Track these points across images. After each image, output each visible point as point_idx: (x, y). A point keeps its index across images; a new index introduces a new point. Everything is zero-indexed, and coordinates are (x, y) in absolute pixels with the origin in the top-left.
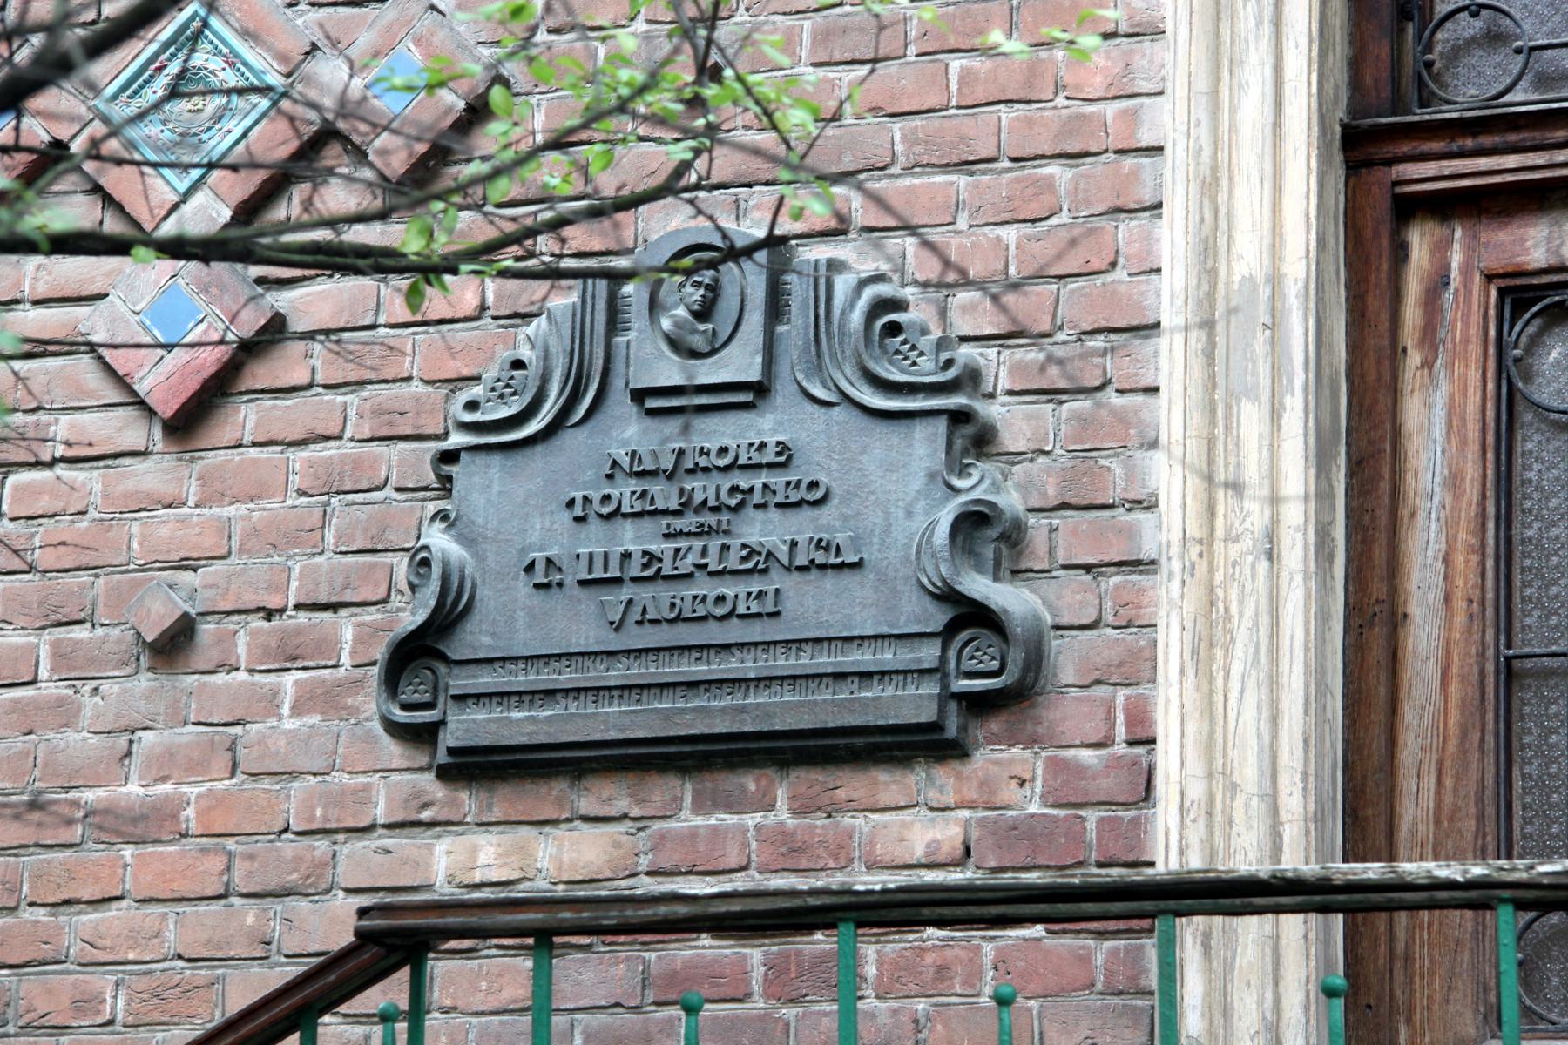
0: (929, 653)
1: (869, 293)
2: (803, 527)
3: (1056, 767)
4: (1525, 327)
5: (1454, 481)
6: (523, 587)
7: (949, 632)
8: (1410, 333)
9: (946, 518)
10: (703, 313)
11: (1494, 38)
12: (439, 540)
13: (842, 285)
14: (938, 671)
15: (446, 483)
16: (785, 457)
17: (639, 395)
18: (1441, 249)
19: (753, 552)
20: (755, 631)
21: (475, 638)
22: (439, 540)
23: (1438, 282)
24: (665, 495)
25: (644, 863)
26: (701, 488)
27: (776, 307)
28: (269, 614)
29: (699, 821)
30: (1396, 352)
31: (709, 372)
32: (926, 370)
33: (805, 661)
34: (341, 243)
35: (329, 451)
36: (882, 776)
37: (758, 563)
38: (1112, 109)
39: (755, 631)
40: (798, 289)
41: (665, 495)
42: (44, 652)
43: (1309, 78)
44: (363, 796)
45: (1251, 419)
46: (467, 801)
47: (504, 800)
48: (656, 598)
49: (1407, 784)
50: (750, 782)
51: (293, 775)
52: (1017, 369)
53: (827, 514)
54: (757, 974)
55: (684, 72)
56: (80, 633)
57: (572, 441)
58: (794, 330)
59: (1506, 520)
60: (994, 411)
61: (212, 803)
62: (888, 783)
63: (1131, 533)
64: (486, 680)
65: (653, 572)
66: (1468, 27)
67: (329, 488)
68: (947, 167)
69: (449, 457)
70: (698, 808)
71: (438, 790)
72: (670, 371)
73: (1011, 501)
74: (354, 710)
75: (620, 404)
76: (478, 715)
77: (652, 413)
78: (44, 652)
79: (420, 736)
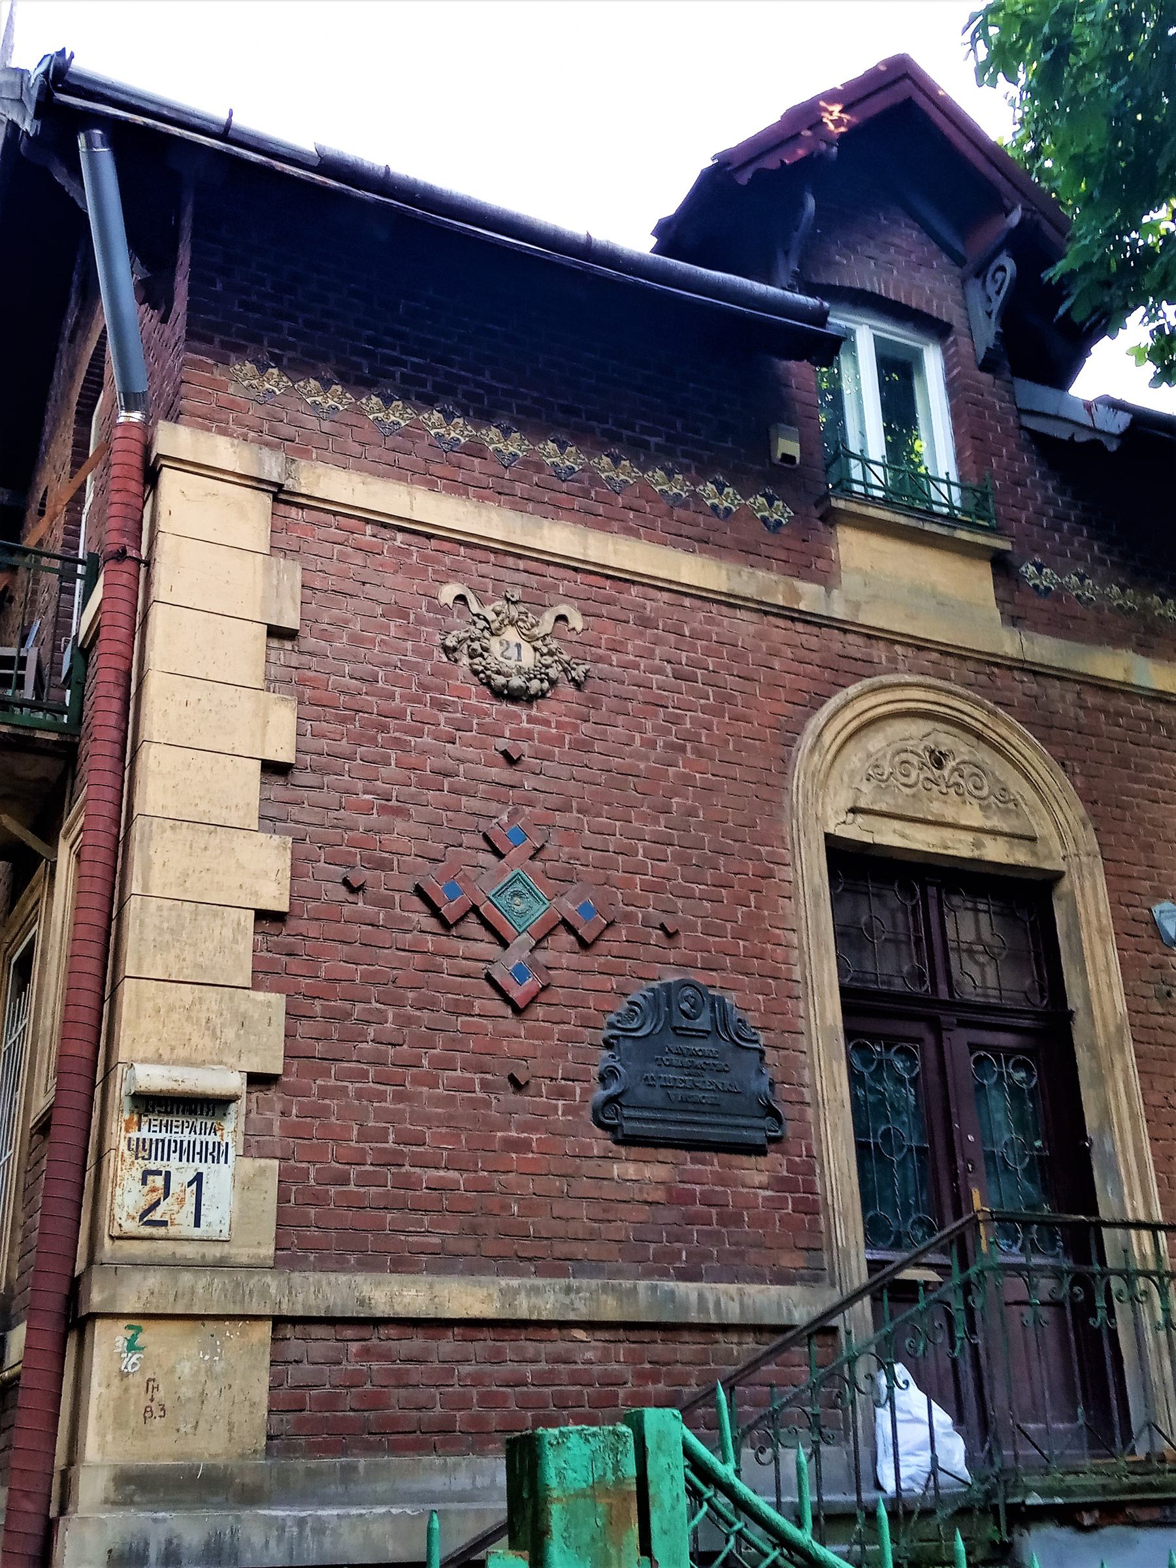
25: (678, 1179)
28: (552, 1079)
29: (692, 1167)
34: (1045, 1190)
35: (566, 1027)
36: (744, 1158)
38: (783, 966)
42: (477, 1081)
43: (850, 722)
46: (623, 1151)
47: (635, 1152)
50: (707, 1155)
51: (566, 1136)
54: (715, 1217)
56: (489, 1076)
62: (744, 1160)
67: (566, 1038)
68: (741, 974)
71: (614, 1147)
74: (581, 1116)
77: (678, 1035)
78: (477, 1081)
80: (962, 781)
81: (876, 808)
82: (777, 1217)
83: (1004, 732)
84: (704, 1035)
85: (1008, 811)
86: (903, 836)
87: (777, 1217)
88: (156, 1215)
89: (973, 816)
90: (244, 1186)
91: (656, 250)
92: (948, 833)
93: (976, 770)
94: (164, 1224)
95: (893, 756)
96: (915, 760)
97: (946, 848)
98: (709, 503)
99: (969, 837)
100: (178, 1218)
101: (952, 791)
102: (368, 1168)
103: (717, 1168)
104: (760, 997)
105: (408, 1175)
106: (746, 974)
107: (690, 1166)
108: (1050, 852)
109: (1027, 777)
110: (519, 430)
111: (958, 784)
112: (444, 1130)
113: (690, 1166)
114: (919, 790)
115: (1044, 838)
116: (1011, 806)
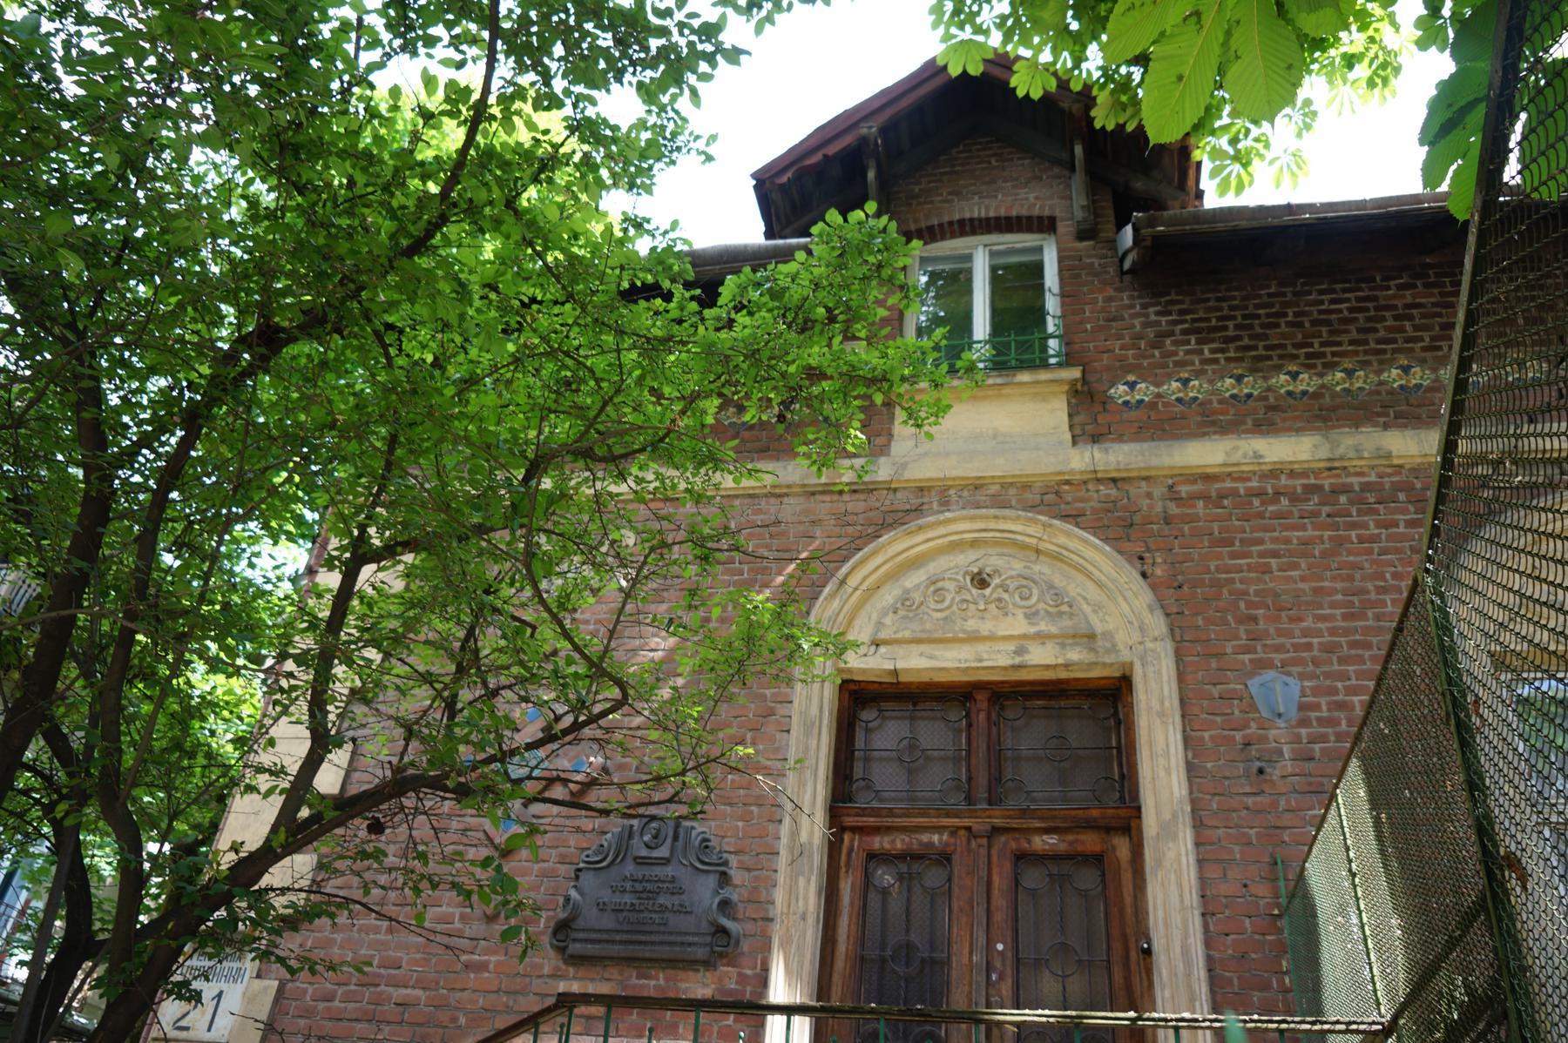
0: (708, 939)
1: (946, 603)
2: (676, 900)
3: (740, 974)
4: (872, 865)
5: (852, 904)
6: (595, 910)
7: (714, 935)
8: (843, 863)
9: (717, 900)
10: (655, 837)
11: (868, 788)
12: (573, 893)
13: (694, 833)
14: (711, 945)
15: (577, 877)
16: (673, 880)
17: (636, 858)
18: (852, 841)
19: (1237, 57)
20: (662, 929)
21: (580, 923)
22: (573, 893)
23: (851, 850)
24: (638, 887)
26: (649, 886)
27: (676, 838)
30: (839, 868)
31: (656, 854)
32: (714, 859)
33: (672, 938)
37: (663, 909)
39: (662, 929)
40: (682, 832)
41: (638, 887)
44: (541, 966)
45: (802, 881)
48: (633, 917)
49: (834, 988)
52: (740, 862)
53: (684, 897)
55: (587, 732)
57: (615, 869)
58: (680, 843)
59: (864, 916)
60: (732, 872)
61: (498, 963)
63: (767, 911)
64: (581, 935)
65: (633, 907)
66: (862, 783)
67: (544, 874)
69: (579, 870)
70: (638, 977)
72: (644, 852)
73: (735, 898)
75: (629, 860)
76: (578, 946)
79: (561, 950)
80: (1006, 596)
81: (899, 635)
82: (716, 1028)
83: (1062, 540)
84: (665, 862)
85: (1061, 614)
86: (931, 657)
87: (716, 1028)
88: (183, 1023)
89: (1017, 625)
90: (249, 998)
91: (769, 234)
92: (982, 648)
93: (1025, 582)
94: (187, 1029)
95: (927, 587)
96: (950, 586)
97: (981, 660)
98: (1283, 391)
99: (1011, 647)
100: (198, 1025)
101: (992, 607)
102: (353, 987)
103: (662, 982)
104: (740, 824)
105: (380, 994)
106: (730, 804)
107: (635, 981)
108: (1114, 646)
109: (1089, 576)
110: (1145, 380)
111: (1000, 600)
112: (418, 956)
113: (635, 981)
114: (953, 613)
115: (1107, 635)
116: (1065, 608)
